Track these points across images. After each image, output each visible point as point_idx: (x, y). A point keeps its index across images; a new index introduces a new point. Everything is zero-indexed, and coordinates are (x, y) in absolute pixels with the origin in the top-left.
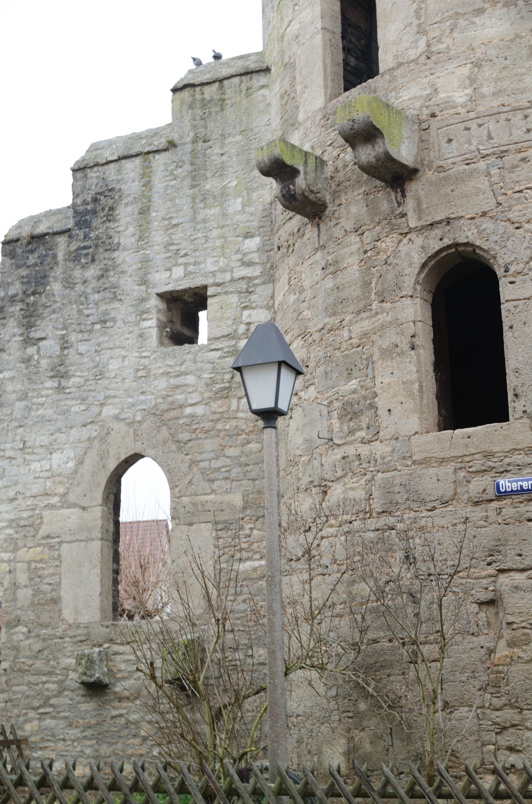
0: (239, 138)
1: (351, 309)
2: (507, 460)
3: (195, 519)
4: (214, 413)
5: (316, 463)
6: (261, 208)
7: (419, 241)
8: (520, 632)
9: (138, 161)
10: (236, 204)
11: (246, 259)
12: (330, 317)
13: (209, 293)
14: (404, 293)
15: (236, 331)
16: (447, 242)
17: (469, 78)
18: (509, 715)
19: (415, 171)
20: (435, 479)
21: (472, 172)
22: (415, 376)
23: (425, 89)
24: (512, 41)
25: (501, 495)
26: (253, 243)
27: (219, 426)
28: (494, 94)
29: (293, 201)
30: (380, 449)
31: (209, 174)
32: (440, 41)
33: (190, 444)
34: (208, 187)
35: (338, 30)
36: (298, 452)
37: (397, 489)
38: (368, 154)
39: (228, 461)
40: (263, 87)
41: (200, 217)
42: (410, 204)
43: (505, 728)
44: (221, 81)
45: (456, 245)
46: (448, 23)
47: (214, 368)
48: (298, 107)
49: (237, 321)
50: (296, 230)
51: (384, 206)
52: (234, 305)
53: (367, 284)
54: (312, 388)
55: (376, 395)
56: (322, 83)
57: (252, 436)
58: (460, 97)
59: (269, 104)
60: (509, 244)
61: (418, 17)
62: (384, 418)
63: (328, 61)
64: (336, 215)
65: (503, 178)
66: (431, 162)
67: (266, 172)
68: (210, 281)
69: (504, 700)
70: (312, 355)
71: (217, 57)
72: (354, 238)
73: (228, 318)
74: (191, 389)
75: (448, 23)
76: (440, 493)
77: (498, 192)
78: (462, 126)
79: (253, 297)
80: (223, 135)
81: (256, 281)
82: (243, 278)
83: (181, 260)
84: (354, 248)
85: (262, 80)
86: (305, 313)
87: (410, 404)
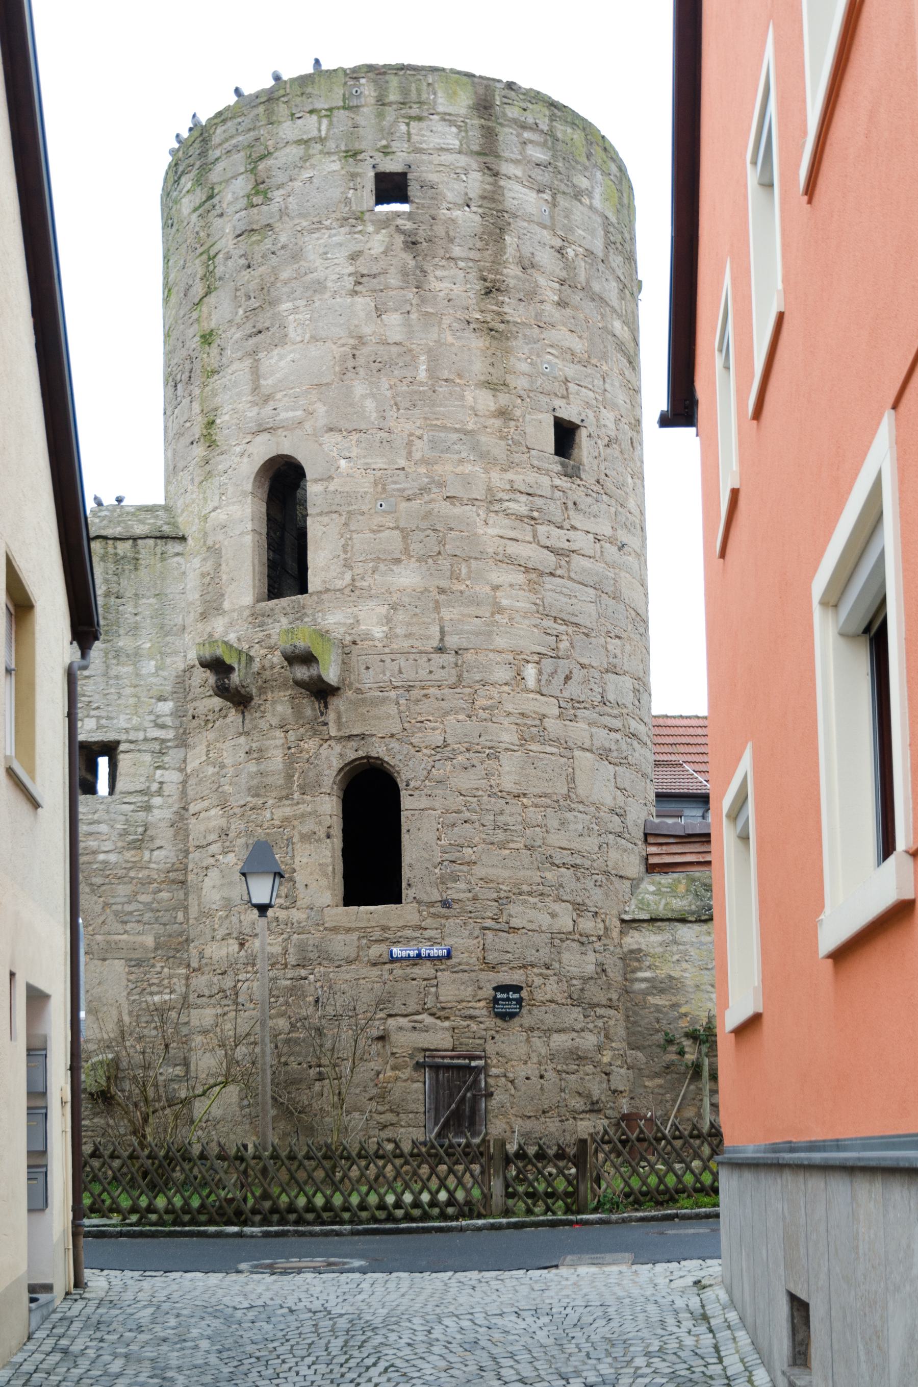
0: (153, 601)
1: (274, 794)
2: (399, 934)
3: (108, 955)
4: (127, 862)
5: (234, 919)
6: (174, 674)
7: (338, 748)
8: (401, 1060)
10: (149, 666)
11: (160, 721)
12: (253, 796)
14: (323, 790)
15: (148, 787)
16: (361, 753)
17: (386, 617)
18: (390, 1117)
19: (338, 689)
20: (342, 943)
21: (385, 699)
22: (329, 860)
23: (349, 618)
24: (422, 593)
25: (393, 960)
26: (167, 707)
27: (132, 874)
28: (406, 636)
29: (223, 691)
30: (296, 915)
31: (122, 631)
32: (363, 578)
33: (104, 888)
34: (121, 644)
35: (264, 531)
36: (214, 907)
37: (310, 948)
38: (302, 672)
39: (141, 907)
40: (177, 554)
41: (113, 673)
42: (331, 716)
43: (385, 1126)
44: (135, 539)
45: (368, 757)
46: (371, 565)
47: (127, 820)
48: (223, 595)
49: (150, 778)
50: (217, 709)
51: (308, 712)
52: (148, 764)
53: (289, 777)
54: (232, 855)
55: (294, 871)
56: (251, 582)
57: (163, 886)
58: (378, 632)
59: (184, 573)
60: (410, 763)
61: (345, 552)
62: (301, 892)
63: (256, 561)
64: (262, 708)
65: (409, 709)
66: (351, 683)
67: (205, 664)
68: (123, 737)
69: (387, 1107)
70: (233, 827)
71: (119, 500)
72: (279, 733)
73: (141, 775)
74: (104, 838)
75: (371, 565)
76: (346, 955)
77: (404, 719)
78: (378, 658)
79: (166, 759)
80: (136, 595)
81: (169, 744)
82: (156, 739)
83: (93, 713)
84: (279, 742)
85: (177, 547)
86: (226, 787)
87: (324, 882)
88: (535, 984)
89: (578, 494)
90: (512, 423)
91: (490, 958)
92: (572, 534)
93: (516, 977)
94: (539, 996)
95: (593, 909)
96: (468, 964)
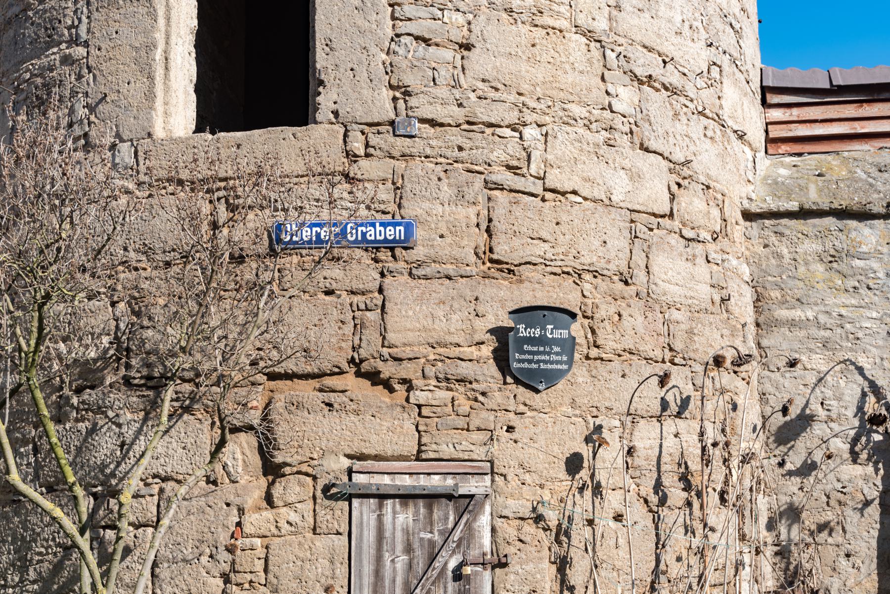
88: (601, 313)
91: (502, 251)
93: (565, 295)
94: (609, 340)
95: (702, 179)
96: (456, 261)
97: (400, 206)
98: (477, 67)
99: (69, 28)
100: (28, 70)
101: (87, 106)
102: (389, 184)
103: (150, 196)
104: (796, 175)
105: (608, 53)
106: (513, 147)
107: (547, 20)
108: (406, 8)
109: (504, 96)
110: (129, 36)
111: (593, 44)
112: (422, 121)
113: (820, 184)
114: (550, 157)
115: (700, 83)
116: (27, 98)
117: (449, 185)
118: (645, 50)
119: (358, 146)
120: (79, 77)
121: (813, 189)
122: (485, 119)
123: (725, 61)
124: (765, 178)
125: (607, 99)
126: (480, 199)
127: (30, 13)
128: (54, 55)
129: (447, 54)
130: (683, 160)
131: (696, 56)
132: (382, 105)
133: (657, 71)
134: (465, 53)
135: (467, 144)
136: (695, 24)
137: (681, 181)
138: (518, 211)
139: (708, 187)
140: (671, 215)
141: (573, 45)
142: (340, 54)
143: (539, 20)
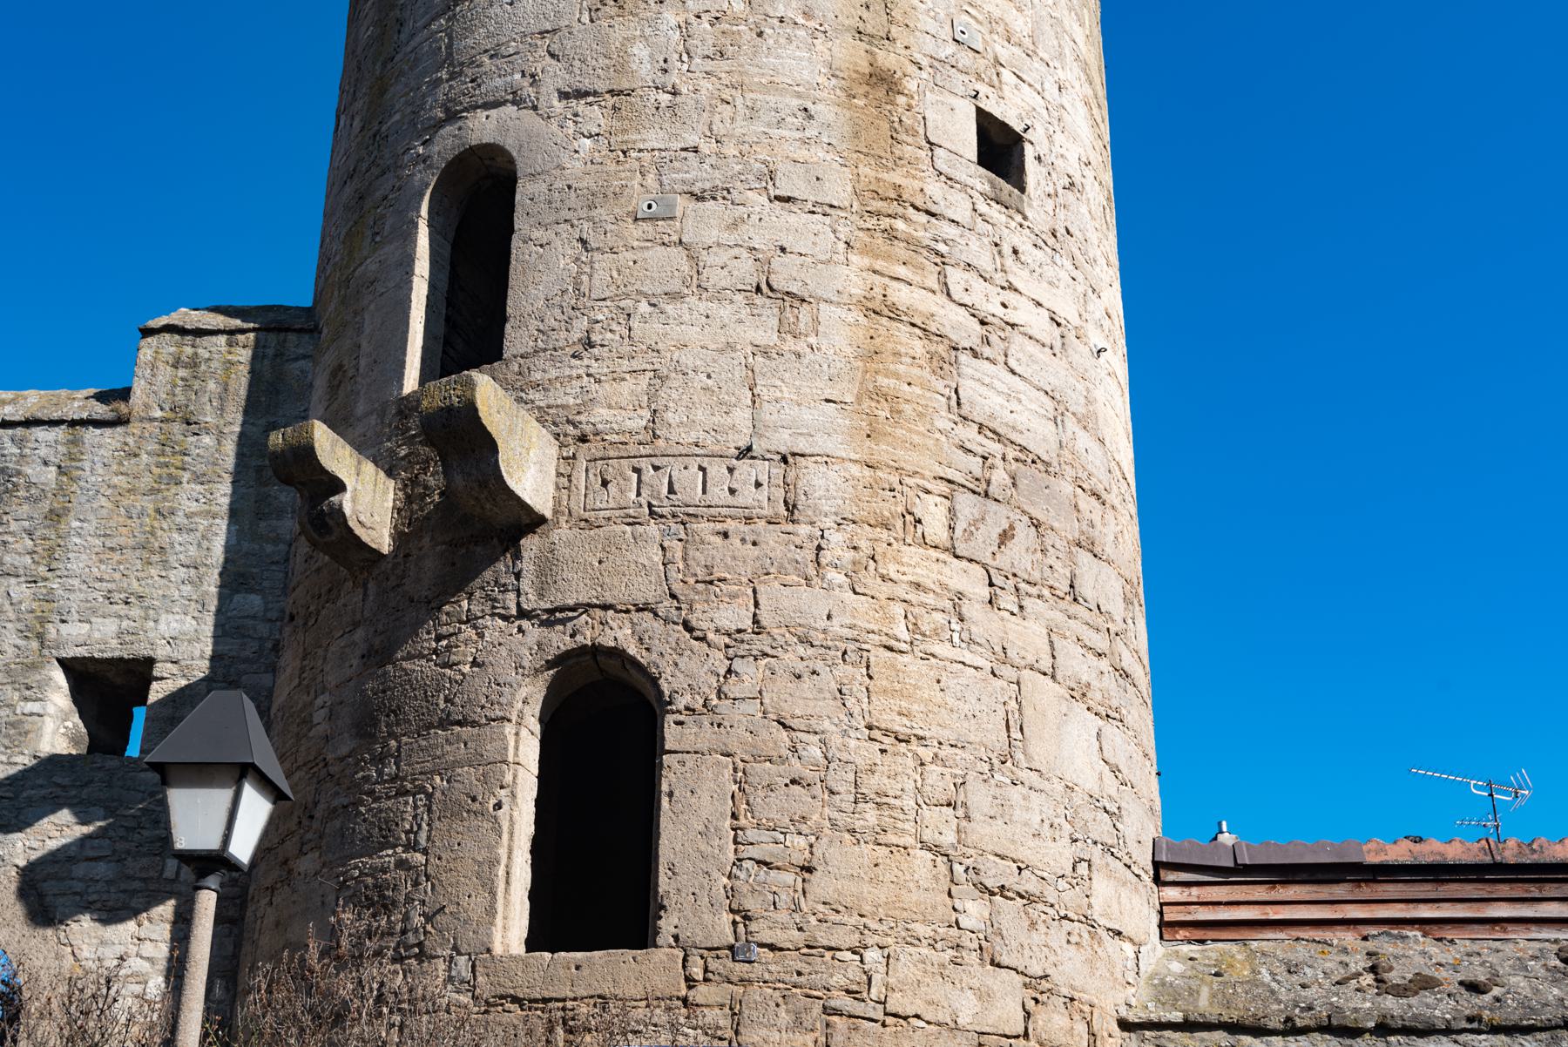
9: (59, 433)
13: (156, 673)
89: (1016, 238)
90: (901, 100)
92: (1009, 297)
95: (1065, 991)
97: (737, 1033)
98: (818, 890)
99: (407, 833)
100: (356, 867)
101: (424, 914)
102: (727, 1010)
103: (486, 1012)
104: (1189, 973)
105: (956, 867)
106: (854, 972)
107: (891, 838)
108: (748, 832)
109: (846, 919)
110: (472, 850)
111: (939, 859)
112: (761, 945)
113: (1215, 987)
114: (891, 980)
115: (1062, 884)
116: (354, 895)
117: (787, 1011)
118: (997, 859)
119: (697, 972)
120: (416, 884)
121: (1205, 992)
122: (826, 943)
123: (1096, 853)
124: (1151, 978)
125: (954, 915)
126: (818, 1025)
127: (363, 809)
128: (388, 857)
129: (789, 878)
130: (1041, 973)
131: (1058, 855)
132: (722, 928)
133: (1011, 880)
134: (807, 875)
135: (806, 969)
136: (1057, 821)
137: (1038, 996)
138: (857, 1038)
139: (1072, 1000)
140: (1026, 1035)
141: (918, 862)
142: (683, 878)
143: (882, 838)
